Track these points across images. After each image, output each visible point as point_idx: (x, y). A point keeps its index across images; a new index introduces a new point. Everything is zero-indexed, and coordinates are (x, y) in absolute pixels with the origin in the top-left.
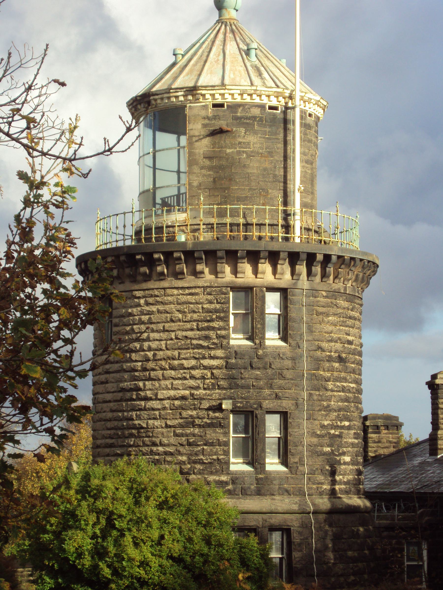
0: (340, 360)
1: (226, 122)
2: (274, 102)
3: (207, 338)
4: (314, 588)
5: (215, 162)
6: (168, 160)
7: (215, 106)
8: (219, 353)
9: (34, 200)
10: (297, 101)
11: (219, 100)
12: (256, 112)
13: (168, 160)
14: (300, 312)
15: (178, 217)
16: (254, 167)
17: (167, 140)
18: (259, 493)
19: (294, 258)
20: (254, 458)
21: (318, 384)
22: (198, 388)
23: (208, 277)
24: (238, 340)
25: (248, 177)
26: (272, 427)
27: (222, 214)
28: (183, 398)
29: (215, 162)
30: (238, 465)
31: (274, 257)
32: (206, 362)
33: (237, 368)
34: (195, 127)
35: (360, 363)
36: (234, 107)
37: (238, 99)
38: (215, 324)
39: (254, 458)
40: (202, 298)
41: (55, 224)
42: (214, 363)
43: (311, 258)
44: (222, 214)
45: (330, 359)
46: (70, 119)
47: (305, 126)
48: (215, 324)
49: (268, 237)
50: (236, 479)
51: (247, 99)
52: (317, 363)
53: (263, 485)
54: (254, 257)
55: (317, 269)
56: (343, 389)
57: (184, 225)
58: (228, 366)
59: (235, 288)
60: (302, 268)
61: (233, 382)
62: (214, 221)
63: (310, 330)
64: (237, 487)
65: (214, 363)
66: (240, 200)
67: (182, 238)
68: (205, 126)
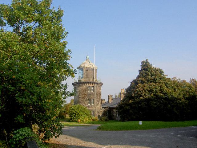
1: (88, 69)
6: (81, 73)
9: (18, 92)
13: (81, 73)
14: (95, 89)
15: (83, 79)
16: (90, 74)
17: (81, 71)
19: (94, 83)
20: (91, 104)
21: (97, 96)
23: (88, 85)
24: (89, 92)
26: (92, 101)
30: (89, 104)
31: (92, 83)
33: (89, 94)
36: (88, 68)
39: (91, 104)
41: (166, 76)
43: (96, 83)
49: (91, 81)
52: (97, 94)
53: (91, 106)
54: (90, 83)
55: (97, 84)
57: (83, 80)
59: (92, 86)
60: (95, 84)
64: (89, 106)
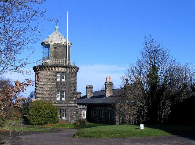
0: (73, 83)
2: (64, 43)
3: (53, 80)
4: (2, 19)
5: (55, 52)
7: (55, 44)
8: (55, 82)
10: (67, 43)
11: (56, 43)
12: (61, 45)
16: (61, 53)
18: (61, 103)
22: (52, 87)
25: (59, 55)
27: (56, 60)
28: (50, 89)
29: (55, 52)
32: (53, 83)
34: (51, 47)
35: (76, 84)
36: (57, 44)
37: (59, 43)
38: (54, 78)
40: (53, 73)
42: (55, 83)
43: (69, 67)
44: (56, 60)
45: (72, 83)
46: (25, 89)
47: (69, 47)
48: (54, 78)
50: (58, 101)
51: (60, 43)
52: (70, 84)
56: (74, 88)
58: (57, 84)
61: (57, 86)
62: (54, 61)
63: (69, 79)
65: (55, 83)
66: (58, 58)
67: (49, 64)
68: (53, 47)
